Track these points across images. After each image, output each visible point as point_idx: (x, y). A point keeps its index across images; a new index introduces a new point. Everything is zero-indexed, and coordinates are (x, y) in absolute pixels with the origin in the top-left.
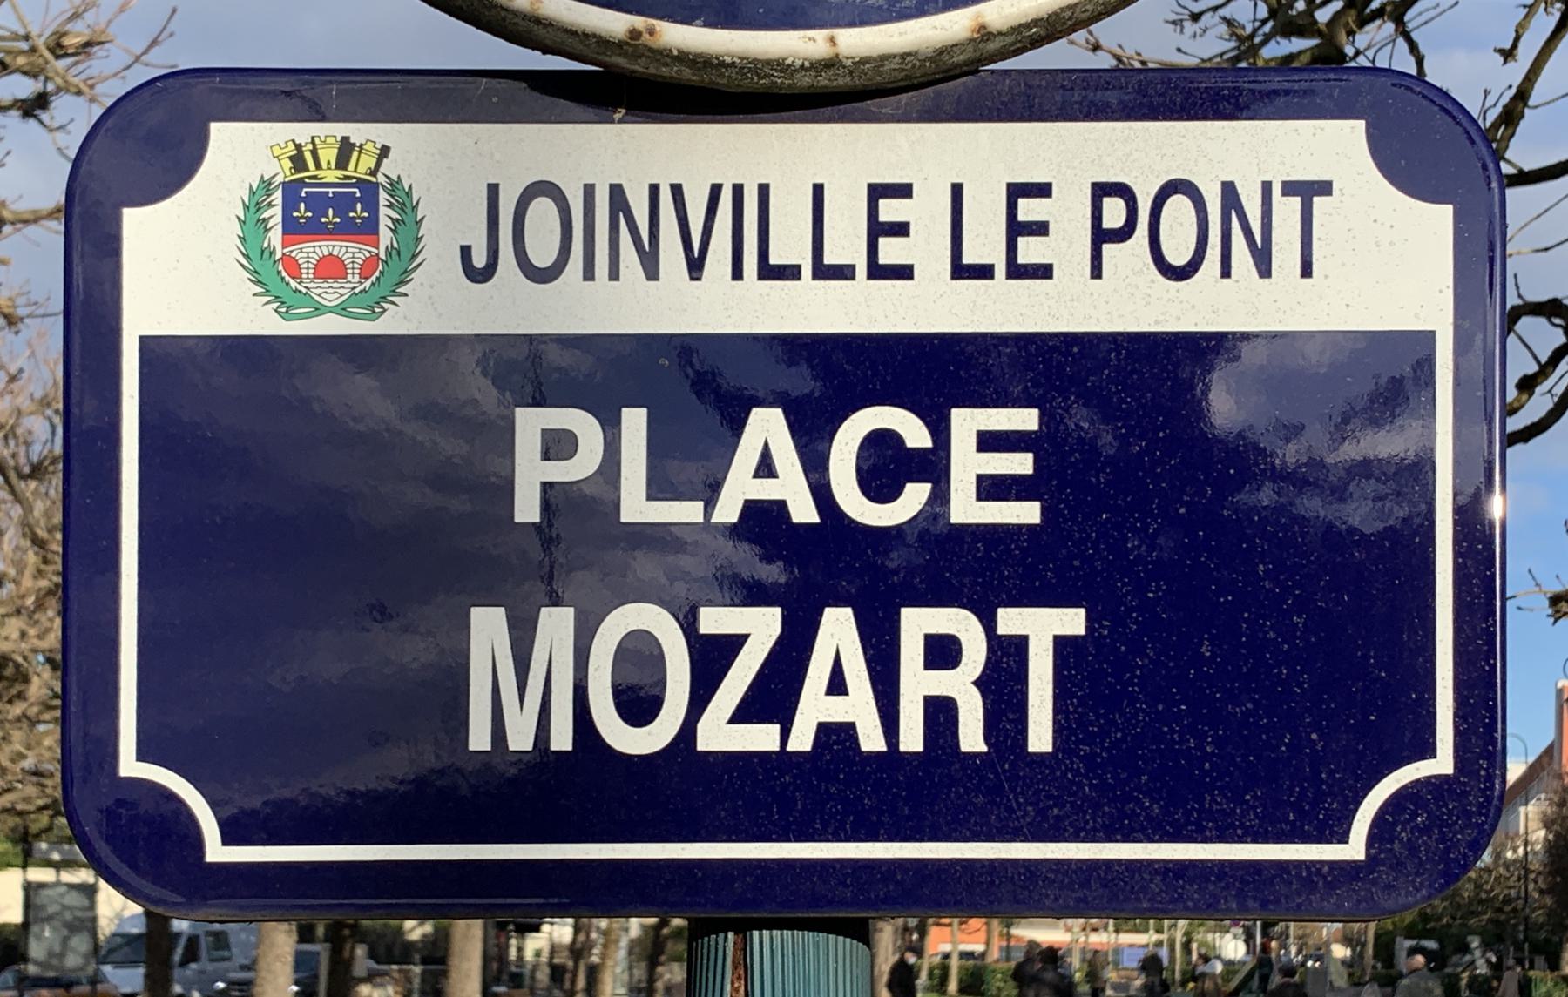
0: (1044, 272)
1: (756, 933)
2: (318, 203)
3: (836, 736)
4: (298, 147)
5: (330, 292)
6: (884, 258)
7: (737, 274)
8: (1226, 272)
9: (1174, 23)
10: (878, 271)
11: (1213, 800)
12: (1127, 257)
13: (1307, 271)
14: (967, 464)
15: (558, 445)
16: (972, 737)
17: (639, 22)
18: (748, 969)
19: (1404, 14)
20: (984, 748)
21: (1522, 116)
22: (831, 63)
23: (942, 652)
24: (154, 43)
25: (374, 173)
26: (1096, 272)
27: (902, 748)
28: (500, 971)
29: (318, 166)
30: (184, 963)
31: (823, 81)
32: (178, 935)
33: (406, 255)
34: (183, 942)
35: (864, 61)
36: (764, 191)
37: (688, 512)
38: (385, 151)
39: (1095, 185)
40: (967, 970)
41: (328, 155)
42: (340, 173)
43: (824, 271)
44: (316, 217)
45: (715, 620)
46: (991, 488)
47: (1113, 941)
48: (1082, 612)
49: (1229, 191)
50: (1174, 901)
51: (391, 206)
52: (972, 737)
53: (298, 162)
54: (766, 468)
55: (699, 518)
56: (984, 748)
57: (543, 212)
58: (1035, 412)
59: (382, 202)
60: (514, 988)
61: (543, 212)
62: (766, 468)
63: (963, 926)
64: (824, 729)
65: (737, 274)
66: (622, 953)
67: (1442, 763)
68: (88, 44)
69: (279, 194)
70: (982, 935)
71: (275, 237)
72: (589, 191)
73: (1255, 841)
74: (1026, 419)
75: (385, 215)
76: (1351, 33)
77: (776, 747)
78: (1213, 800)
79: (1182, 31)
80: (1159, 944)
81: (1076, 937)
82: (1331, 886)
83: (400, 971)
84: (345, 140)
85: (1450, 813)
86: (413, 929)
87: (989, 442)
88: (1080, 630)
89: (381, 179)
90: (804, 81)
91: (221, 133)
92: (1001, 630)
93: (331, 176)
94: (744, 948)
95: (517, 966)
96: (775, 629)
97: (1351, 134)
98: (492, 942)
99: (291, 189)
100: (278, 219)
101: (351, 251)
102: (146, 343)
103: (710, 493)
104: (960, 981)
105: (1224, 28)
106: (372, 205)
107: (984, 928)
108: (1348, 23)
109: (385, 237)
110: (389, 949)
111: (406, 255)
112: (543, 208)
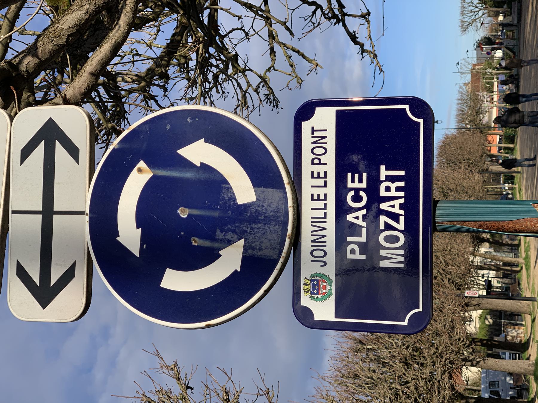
0: (325, 173)
1: (436, 220)
2: (314, 289)
3: (402, 206)
4: (305, 292)
5: (328, 288)
6: (323, 198)
7: (325, 222)
8: (326, 143)
9: (225, 98)
10: (325, 199)
11: (413, 144)
12: (323, 159)
13: (326, 130)
14: (357, 185)
15: (353, 252)
16: (402, 184)
17: (287, 237)
18: (442, 222)
19: (222, 35)
20: (404, 182)
21: (250, 4)
22: (293, 207)
23: (388, 189)
24: (226, 374)
25: (309, 280)
26: (326, 164)
27: (404, 196)
28: (504, 294)
29: (308, 289)
30: (499, 396)
31: (296, 208)
32: (489, 396)
33: (322, 275)
34: (491, 395)
35: (293, 202)
36: (312, 218)
37: (364, 231)
38: (306, 278)
39: (312, 164)
40: (505, 141)
41: (306, 287)
42: (309, 285)
43: (325, 208)
44: (316, 289)
45: (382, 226)
46: (361, 181)
47: (496, 93)
48: (381, 166)
49: (313, 143)
50: (430, 151)
51: (314, 278)
52: (402, 184)
53: (307, 292)
54: (357, 218)
55: (365, 229)
56: (404, 182)
57: (315, 253)
58: (348, 174)
59: (314, 279)
60: (510, 290)
61: (315, 253)
62: (357, 218)
63: (491, 142)
64: (401, 208)
65: (325, 222)
66: (498, 254)
67: (407, 107)
68: (226, 392)
69: (312, 295)
70: (494, 136)
71: (319, 296)
72: (312, 246)
73: (420, 137)
74: (349, 175)
75: (316, 278)
76: (229, 53)
77: (404, 216)
78: (413, 144)
79: (227, 96)
80: (497, 78)
81: (495, 106)
82: (428, 125)
83: (504, 327)
84: (304, 284)
85: (415, 105)
86: (489, 322)
87: (353, 181)
88: (384, 166)
89: (310, 279)
90: (296, 211)
91: (303, 304)
92: (384, 179)
93: (309, 287)
94: (439, 222)
95: (503, 289)
96: (384, 216)
97: (304, 124)
98: (494, 296)
99: (312, 293)
100: (316, 295)
101: (321, 284)
102: (336, 317)
103: (361, 227)
104: (510, 143)
105: (224, 83)
106: (314, 280)
107: (492, 135)
108: (227, 53)
109: (319, 279)
110: (496, 330)
111: (322, 275)
112: (315, 253)
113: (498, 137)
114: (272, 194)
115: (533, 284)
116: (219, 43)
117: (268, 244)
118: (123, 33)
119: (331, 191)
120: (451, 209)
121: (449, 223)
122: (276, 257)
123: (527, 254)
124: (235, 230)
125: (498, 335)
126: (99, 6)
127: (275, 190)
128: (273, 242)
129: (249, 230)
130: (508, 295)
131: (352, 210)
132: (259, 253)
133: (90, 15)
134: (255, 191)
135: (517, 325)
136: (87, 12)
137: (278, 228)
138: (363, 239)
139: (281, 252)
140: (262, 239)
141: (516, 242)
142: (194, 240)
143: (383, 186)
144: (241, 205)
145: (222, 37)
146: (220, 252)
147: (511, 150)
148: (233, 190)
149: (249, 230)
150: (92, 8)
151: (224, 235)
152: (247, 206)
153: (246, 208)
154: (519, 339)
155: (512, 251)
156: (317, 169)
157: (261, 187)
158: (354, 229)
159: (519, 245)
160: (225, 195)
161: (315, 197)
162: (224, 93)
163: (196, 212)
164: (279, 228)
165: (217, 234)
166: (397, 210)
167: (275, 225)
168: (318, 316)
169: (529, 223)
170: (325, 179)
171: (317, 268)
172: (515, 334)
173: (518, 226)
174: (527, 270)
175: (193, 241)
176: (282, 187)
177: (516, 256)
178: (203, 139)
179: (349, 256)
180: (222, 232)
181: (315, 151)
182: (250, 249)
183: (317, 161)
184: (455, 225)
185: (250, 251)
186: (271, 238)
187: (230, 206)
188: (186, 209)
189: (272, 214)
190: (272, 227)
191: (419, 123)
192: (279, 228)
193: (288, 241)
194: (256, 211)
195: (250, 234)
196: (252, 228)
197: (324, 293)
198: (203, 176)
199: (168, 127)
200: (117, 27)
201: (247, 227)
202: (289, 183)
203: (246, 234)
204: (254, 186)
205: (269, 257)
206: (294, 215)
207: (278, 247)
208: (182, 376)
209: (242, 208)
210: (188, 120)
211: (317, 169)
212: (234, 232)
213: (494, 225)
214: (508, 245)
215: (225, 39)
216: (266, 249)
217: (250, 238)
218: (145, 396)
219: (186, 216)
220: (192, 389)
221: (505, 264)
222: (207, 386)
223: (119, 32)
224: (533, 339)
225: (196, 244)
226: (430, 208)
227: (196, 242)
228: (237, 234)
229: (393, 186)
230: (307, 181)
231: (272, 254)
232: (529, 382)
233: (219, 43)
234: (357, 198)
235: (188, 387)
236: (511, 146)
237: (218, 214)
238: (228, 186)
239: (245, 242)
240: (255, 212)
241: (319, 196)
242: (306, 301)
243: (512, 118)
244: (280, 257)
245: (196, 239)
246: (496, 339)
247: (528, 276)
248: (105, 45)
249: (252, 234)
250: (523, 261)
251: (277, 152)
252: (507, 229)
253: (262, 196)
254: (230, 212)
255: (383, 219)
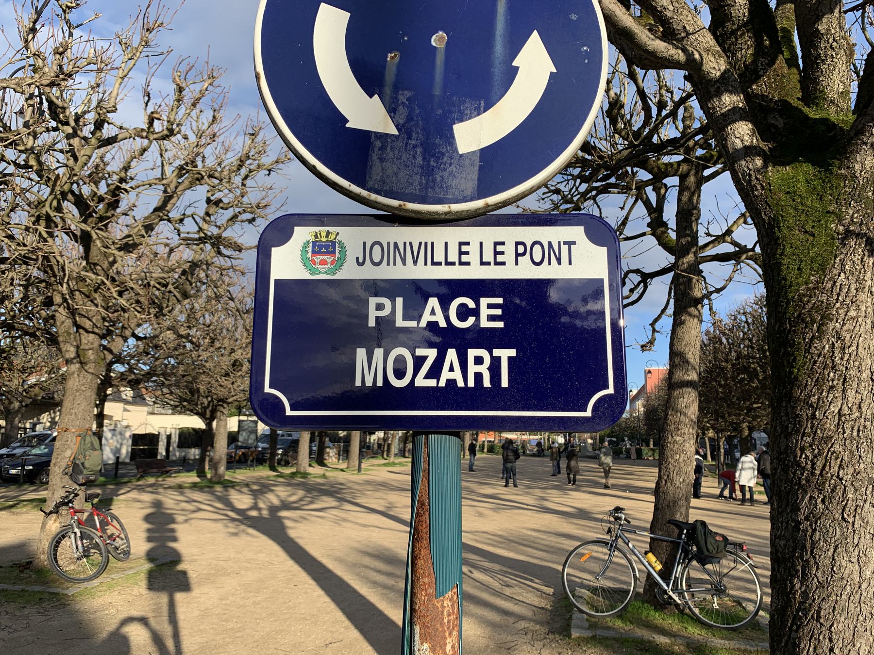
2: (321, 246)
3: (451, 383)
7: (426, 264)
8: (550, 264)
12: (525, 260)
13: (570, 263)
14: (484, 312)
15: (380, 307)
16: (487, 383)
17: (402, 203)
18: (428, 445)
22: (449, 213)
23: (479, 361)
26: (517, 264)
31: (447, 217)
33: (342, 259)
35: (457, 212)
36: (432, 244)
37: (413, 324)
38: (338, 234)
41: (324, 235)
43: (447, 263)
45: (420, 352)
46: (491, 318)
49: (550, 244)
52: (487, 383)
53: (316, 236)
54: (433, 312)
57: (377, 249)
61: (377, 249)
62: (433, 312)
64: (448, 381)
65: (426, 264)
66: (397, 440)
67: (611, 390)
70: (493, 436)
71: (310, 254)
72: (389, 243)
74: (500, 301)
75: (337, 249)
76: (582, 203)
80: (541, 439)
82: (583, 423)
84: (328, 231)
87: (490, 306)
90: (443, 217)
93: (324, 240)
94: (427, 439)
97: (580, 229)
99: (314, 243)
101: (329, 258)
102: (276, 280)
103: (419, 319)
106: (334, 247)
109: (337, 254)
110: (335, 439)
111: (342, 259)
113: (493, 439)
114: (469, 180)
115: (372, 470)
116: (588, 196)
117: (389, 172)
118: (645, 44)
119: (475, 272)
120: (448, 459)
121: (426, 456)
122: (370, 184)
123: (397, 464)
124: (412, 120)
125: (330, 440)
126: (671, 23)
127: (476, 183)
128: (394, 179)
129: (413, 142)
130: (364, 448)
131: (445, 306)
132: (375, 157)
133: (661, 12)
134: (473, 152)
135: (339, 455)
136: (665, 8)
137: (415, 188)
138: (400, 322)
139: (378, 192)
140: (398, 162)
141: (407, 454)
142: (395, 55)
143: (483, 353)
144: (452, 129)
145: (594, 198)
146: (376, 96)
147: (482, 449)
148: (475, 117)
149: (413, 142)
150: (669, 14)
151: (403, 103)
152: (450, 139)
153: (447, 137)
154: (327, 458)
155: (400, 450)
156: (509, 250)
157: (480, 162)
158: (413, 311)
159: (404, 456)
160: (468, 105)
161: (464, 248)
162: (543, 199)
163: (440, 59)
164: (416, 190)
165: (406, 92)
166: (446, 375)
167: (421, 184)
168: (276, 253)
169: (427, 580)
170: (492, 263)
171: (354, 251)
172: (331, 454)
173: (423, 563)
174: (384, 465)
175: (393, 55)
176: (481, 194)
177: (396, 455)
178: (555, 71)
179: (373, 301)
180: (408, 99)
181: (537, 248)
182: (382, 143)
183: (521, 250)
184: (423, 465)
185: (378, 144)
186: (400, 176)
187: (451, 112)
188: (444, 43)
189: (439, 179)
190: (417, 178)
191: (585, 411)
192: (416, 190)
193: (395, 203)
194: (443, 154)
195: (407, 143)
196: (415, 147)
197: (314, 262)
198: (497, 71)
199: (574, 17)
200: (652, 36)
201: (417, 140)
202: (487, 205)
203: (406, 137)
204: (482, 150)
205: (370, 174)
206: (437, 213)
207: (386, 188)
208: (280, 166)
209: (448, 131)
210: (585, 48)
211: (509, 250)
212: (409, 118)
213: (424, 526)
214: (405, 447)
215: (592, 201)
216: (383, 169)
217: (400, 144)
218: (260, 129)
219: (433, 44)
220: (269, 175)
221: (389, 446)
222: (271, 188)
223: (647, 39)
224: (327, 470)
225: (388, 59)
226: (450, 427)
227: (392, 58)
228: (405, 123)
229: (484, 369)
230: (488, 235)
231: (375, 177)
232: (291, 466)
233: (588, 196)
234: (464, 313)
235: (270, 170)
236: (486, 450)
237: (437, 93)
238: (482, 109)
239: (393, 135)
240: (440, 152)
241: (467, 253)
242: (302, 234)
243: (510, 454)
244: (369, 190)
245: (397, 59)
246: (327, 439)
247: (379, 465)
248: (633, 21)
249: (406, 147)
250: (391, 461)
251: (535, 187)
252: (418, 546)
253: (467, 163)
254: (440, 112)
255: (432, 354)
